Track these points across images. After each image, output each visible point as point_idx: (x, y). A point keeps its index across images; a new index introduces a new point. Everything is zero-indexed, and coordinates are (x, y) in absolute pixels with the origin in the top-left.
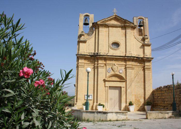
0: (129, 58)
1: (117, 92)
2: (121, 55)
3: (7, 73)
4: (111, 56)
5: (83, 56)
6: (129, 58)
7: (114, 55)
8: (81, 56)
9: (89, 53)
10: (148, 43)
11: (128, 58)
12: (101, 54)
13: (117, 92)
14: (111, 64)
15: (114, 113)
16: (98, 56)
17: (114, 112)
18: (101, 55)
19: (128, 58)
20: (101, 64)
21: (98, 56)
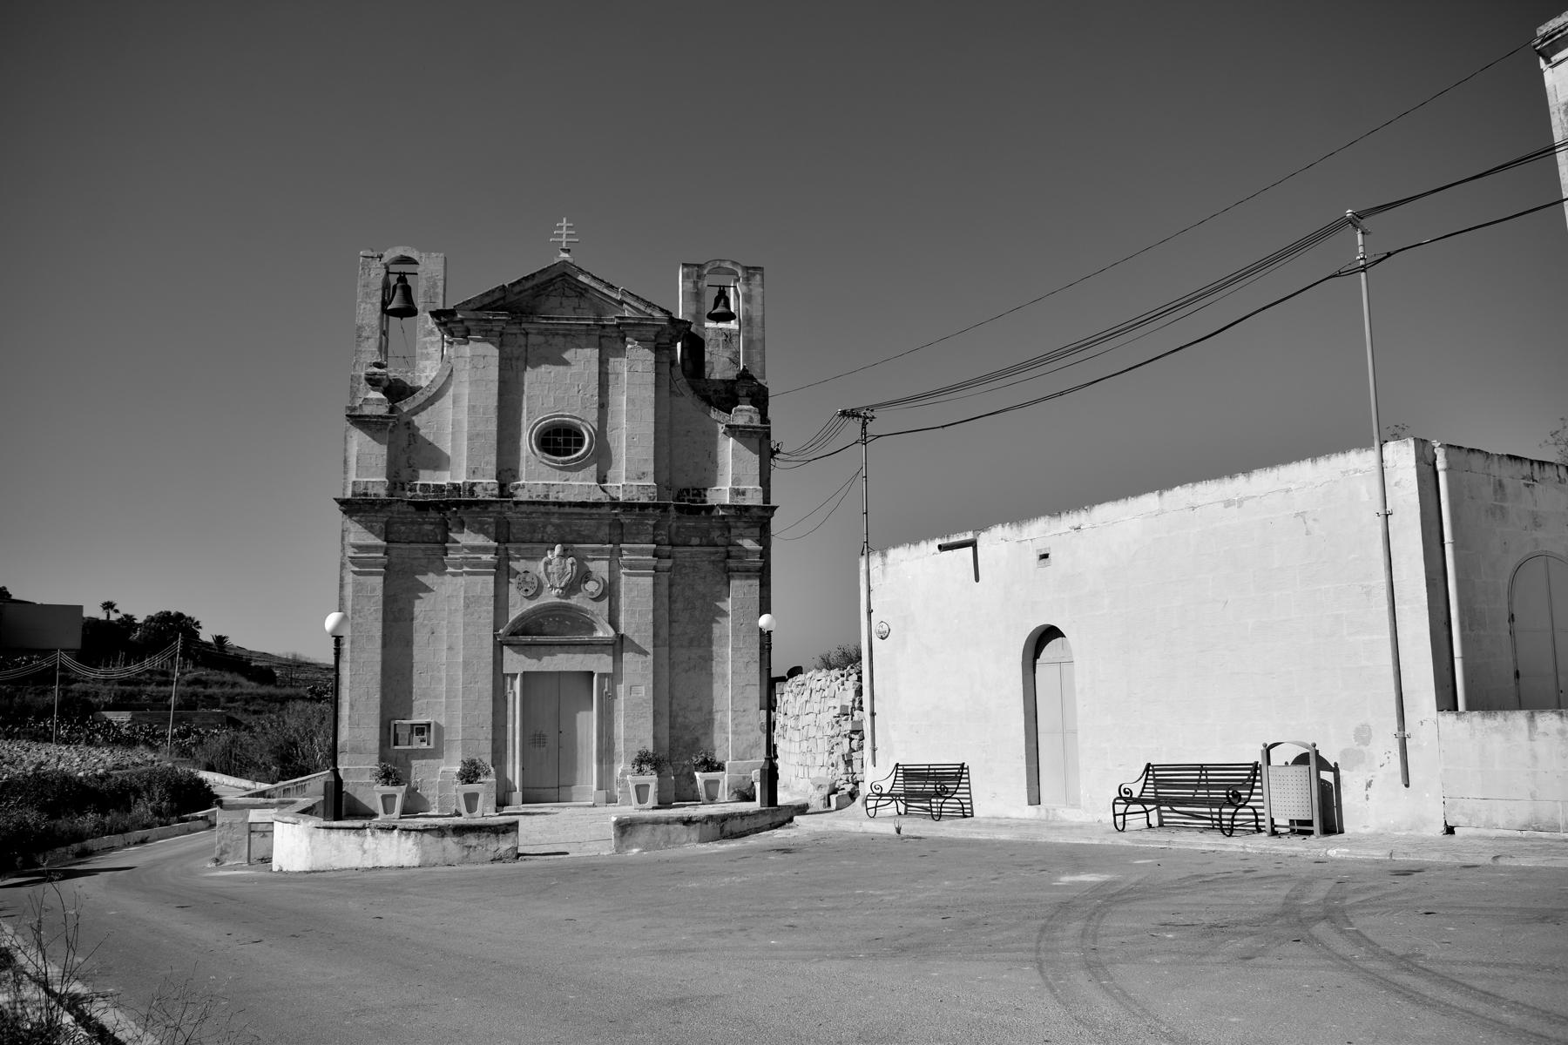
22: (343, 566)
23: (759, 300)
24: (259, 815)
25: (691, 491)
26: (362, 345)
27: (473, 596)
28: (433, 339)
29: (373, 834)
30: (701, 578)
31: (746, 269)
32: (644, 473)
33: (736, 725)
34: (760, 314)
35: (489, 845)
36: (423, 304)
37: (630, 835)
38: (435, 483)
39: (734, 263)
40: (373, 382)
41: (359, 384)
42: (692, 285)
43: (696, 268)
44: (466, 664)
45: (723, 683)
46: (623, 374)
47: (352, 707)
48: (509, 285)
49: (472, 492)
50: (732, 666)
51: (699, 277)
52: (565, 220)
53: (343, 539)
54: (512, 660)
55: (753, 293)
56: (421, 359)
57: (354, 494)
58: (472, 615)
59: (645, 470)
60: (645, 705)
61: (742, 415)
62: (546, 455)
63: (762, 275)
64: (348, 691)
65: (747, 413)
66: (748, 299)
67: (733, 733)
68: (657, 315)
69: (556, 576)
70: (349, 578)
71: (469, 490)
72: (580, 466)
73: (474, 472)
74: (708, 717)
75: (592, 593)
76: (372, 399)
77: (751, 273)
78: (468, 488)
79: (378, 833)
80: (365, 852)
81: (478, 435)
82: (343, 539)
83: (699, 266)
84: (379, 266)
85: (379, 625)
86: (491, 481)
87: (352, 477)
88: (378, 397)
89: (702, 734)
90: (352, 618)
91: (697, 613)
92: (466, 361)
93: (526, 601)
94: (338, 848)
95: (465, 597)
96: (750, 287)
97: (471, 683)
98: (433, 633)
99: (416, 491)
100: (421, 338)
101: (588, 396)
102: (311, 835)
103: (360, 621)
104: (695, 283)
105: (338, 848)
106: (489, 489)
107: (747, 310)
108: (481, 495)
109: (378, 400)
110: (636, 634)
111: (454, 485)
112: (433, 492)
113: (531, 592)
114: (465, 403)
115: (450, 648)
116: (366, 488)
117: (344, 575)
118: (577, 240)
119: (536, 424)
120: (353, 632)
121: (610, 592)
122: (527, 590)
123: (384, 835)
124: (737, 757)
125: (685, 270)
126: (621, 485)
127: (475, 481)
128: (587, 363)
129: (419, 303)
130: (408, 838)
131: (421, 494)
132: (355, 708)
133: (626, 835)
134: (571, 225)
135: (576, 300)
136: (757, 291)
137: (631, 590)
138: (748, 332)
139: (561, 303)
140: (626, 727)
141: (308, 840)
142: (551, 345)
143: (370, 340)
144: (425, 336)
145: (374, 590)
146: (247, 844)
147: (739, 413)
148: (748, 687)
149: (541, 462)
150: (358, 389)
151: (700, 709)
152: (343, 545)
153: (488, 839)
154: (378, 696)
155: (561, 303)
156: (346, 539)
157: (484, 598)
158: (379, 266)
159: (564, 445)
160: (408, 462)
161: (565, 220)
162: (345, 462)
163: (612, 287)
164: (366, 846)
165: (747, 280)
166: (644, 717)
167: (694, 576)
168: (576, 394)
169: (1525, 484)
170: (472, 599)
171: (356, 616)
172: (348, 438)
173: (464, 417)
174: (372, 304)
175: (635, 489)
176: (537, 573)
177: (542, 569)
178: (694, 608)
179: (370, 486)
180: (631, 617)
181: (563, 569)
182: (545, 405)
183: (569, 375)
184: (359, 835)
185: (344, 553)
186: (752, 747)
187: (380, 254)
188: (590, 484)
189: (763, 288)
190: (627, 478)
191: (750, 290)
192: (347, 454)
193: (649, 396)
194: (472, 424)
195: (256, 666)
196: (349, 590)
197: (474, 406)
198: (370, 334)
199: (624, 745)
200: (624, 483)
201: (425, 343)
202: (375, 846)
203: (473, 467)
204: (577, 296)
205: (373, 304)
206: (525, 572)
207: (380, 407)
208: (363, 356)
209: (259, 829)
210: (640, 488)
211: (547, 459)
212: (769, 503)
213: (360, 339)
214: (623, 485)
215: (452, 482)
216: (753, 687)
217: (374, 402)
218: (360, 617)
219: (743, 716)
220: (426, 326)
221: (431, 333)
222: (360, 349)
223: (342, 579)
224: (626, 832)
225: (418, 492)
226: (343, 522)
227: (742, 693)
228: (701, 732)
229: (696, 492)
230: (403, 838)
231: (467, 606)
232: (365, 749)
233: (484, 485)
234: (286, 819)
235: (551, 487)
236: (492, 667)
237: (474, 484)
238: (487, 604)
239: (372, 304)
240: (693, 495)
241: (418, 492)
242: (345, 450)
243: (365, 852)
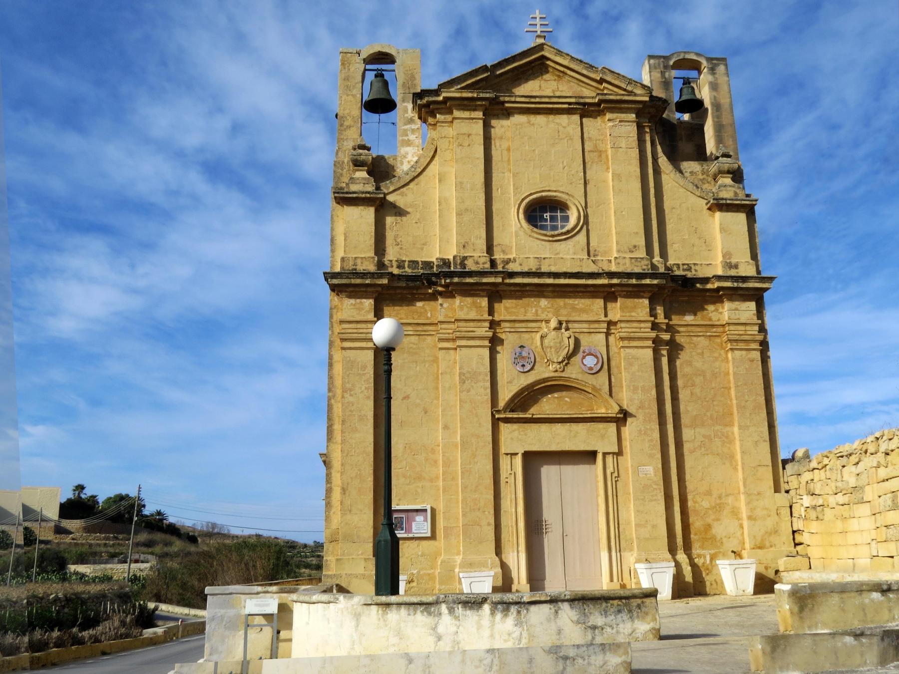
0: (634, 281)
1: (549, 473)
2: (628, 268)
3: (434, 361)
4: (556, 275)
5: (368, 281)
6: (634, 281)
7: (544, 269)
8: (353, 281)
9: (399, 267)
10: (736, 194)
11: (625, 281)
12: (513, 267)
13: (549, 473)
14: (527, 321)
15: (563, 601)
16: (456, 280)
17: (562, 597)
18: (471, 274)
19: (625, 281)
20: (472, 324)
21: (456, 280)
22: (331, 344)
23: (726, 88)
24: (256, 605)
25: (681, 266)
26: (344, 133)
27: (469, 372)
28: (413, 126)
29: (451, 611)
30: (698, 354)
31: (709, 60)
32: (635, 247)
33: (752, 510)
34: (728, 100)
35: (621, 626)
36: (402, 95)
37: (812, 610)
38: (423, 260)
39: (698, 54)
40: (358, 164)
41: (342, 170)
42: (659, 75)
43: (662, 60)
44: (465, 444)
45: (731, 465)
46: (606, 151)
47: (344, 490)
48: (491, 66)
49: (463, 265)
50: (741, 446)
51: (666, 67)
52: (537, 12)
53: (331, 317)
54: (512, 439)
55: (719, 81)
56: (403, 146)
57: (342, 268)
58: (469, 391)
59: (637, 244)
60: (655, 487)
61: (726, 190)
62: (535, 230)
63: (726, 65)
64: (339, 475)
65: (730, 188)
66: (714, 87)
67: (750, 518)
68: (639, 91)
69: (553, 350)
70: (338, 356)
71: (460, 264)
72: (570, 234)
73: (464, 246)
74: (718, 501)
75: (591, 368)
76: (358, 179)
77: (715, 64)
78: (459, 262)
79: (460, 610)
80: (439, 638)
81: (467, 210)
82: (331, 317)
83: (664, 57)
84: (358, 61)
85: (371, 403)
86: (481, 255)
87: (340, 253)
88: (364, 176)
89: (713, 520)
90: (343, 397)
91: (697, 390)
92: (450, 141)
93: (523, 376)
94: (399, 634)
95: (460, 374)
96: (716, 76)
97: (470, 463)
98: (426, 413)
99: (404, 268)
100: (401, 127)
101: (573, 172)
102: (357, 616)
103: (351, 399)
104: (663, 73)
105: (399, 634)
106: (481, 263)
107: (715, 97)
108: (471, 266)
109: (363, 178)
110: (640, 411)
111: (443, 260)
112: (422, 268)
113: (528, 367)
114: (452, 180)
115: (446, 427)
116: (355, 265)
117: (333, 353)
118: (551, 30)
119: (523, 200)
120: (343, 411)
121: (607, 365)
122: (523, 366)
123: (468, 612)
124: (756, 545)
125: (652, 61)
126: (613, 259)
127: (466, 255)
128: (570, 142)
129: (397, 94)
130: (506, 616)
131: (410, 271)
132: (347, 493)
133: (807, 610)
134: (544, 16)
135: (555, 83)
136: (722, 80)
137: (631, 365)
138: (718, 117)
139: (540, 87)
140: (638, 512)
141: (353, 623)
142: (533, 124)
143: (352, 129)
144: (405, 124)
145: (364, 367)
146: (242, 642)
147: (722, 188)
148: (759, 468)
149: (530, 236)
150: (341, 175)
151: (709, 493)
152: (331, 323)
153: (619, 616)
154: (371, 479)
155: (540, 87)
156: (335, 317)
157: (480, 374)
158: (358, 61)
159: (550, 222)
160: (395, 240)
161: (537, 12)
162: (332, 240)
163: (591, 67)
164: (441, 629)
165: (712, 70)
166: (655, 500)
167: (691, 352)
168: (561, 170)
169: (721, 494)
170: (468, 375)
171: (346, 395)
172: (335, 218)
173: (452, 193)
174: (352, 95)
175: (628, 261)
176: (533, 348)
177: (539, 343)
178: (693, 385)
179: (359, 261)
180: (634, 393)
181: (560, 343)
182: (531, 181)
183: (553, 152)
184: (430, 614)
185: (332, 331)
186: (771, 534)
187: (358, 50)
188: (581, 257)
189: (728, 76)
190: (618, 251)
191: (716, 79)
192: (334, 233)
193: (635, 171)
194: (460, 201)
195: (674, 63)
196: (338, 368)
197: (461, 183)
198: (352, 123)
199: (636, 530)
200: (616, 255)
201: (406, 130)
202: (454, 629)
203: (463, 241)
204: (555, 80)
205: (354, 96)
206: (521, 347)
207: (366, 185)
208: (345, 143)
209: (256, 623)
210: (633, 260)
211: (537, 233)
212: (760, 274)
213: (342, 128)
214: (616, 258)
215: (441, 257)
216: (765, 468)
217: (361, 182)
218: (351, 395)
219: (757, 500)
220: (406, 115)
221: (411, 121)
222: (342, 137)
223: (331, 357)
224: (806, 605)
225: (407, 269)
226: (331, 300)
227: (754, 474)
228: (713, 517)
229: (685, 267)
230: (499, 616)
231: (462, 382)
232: (358, 537)
233: (476, 258)
234: (315, 598)
235: (543, 261)
236: (491, 446)
237: (465, 258)
238: (484, 380)
239: (352, 95)
240: (684, 270)
241: (407, 269)
242: (332, 229)
243: (439, 638)
